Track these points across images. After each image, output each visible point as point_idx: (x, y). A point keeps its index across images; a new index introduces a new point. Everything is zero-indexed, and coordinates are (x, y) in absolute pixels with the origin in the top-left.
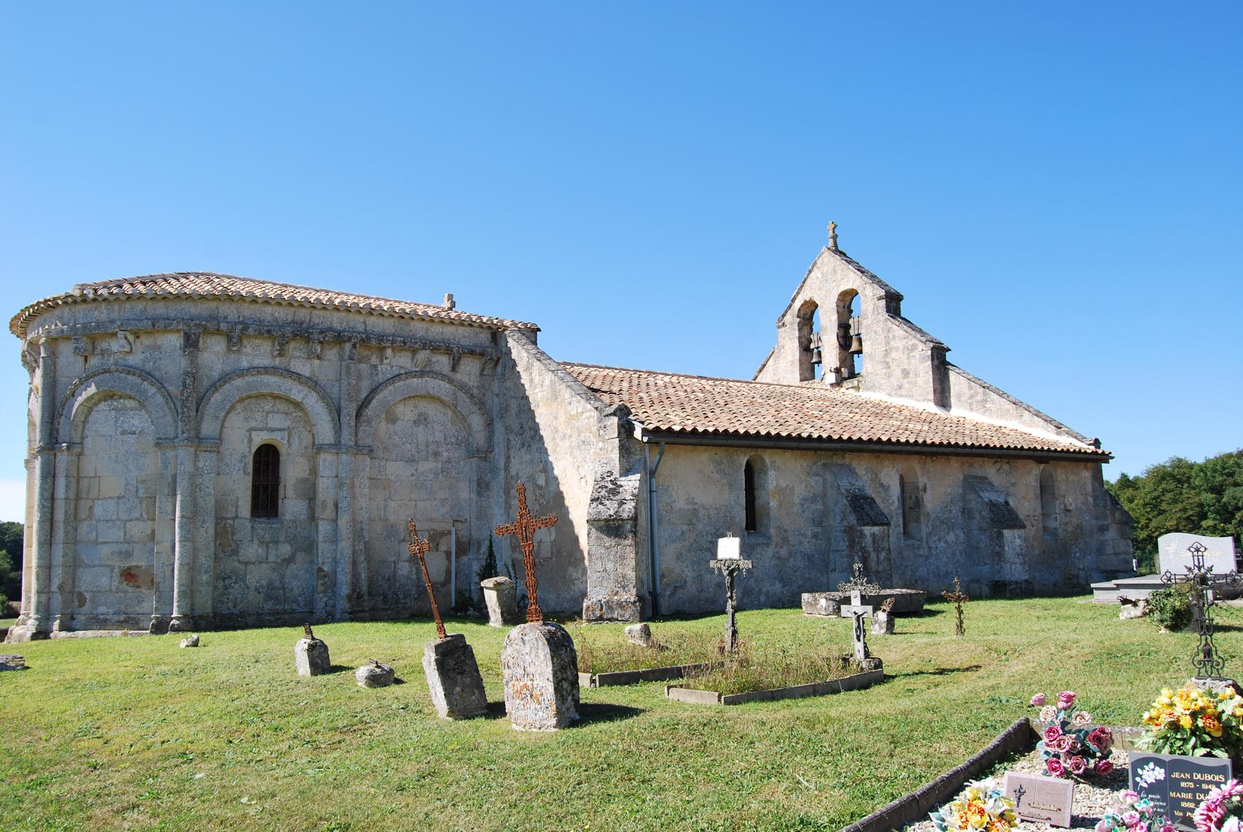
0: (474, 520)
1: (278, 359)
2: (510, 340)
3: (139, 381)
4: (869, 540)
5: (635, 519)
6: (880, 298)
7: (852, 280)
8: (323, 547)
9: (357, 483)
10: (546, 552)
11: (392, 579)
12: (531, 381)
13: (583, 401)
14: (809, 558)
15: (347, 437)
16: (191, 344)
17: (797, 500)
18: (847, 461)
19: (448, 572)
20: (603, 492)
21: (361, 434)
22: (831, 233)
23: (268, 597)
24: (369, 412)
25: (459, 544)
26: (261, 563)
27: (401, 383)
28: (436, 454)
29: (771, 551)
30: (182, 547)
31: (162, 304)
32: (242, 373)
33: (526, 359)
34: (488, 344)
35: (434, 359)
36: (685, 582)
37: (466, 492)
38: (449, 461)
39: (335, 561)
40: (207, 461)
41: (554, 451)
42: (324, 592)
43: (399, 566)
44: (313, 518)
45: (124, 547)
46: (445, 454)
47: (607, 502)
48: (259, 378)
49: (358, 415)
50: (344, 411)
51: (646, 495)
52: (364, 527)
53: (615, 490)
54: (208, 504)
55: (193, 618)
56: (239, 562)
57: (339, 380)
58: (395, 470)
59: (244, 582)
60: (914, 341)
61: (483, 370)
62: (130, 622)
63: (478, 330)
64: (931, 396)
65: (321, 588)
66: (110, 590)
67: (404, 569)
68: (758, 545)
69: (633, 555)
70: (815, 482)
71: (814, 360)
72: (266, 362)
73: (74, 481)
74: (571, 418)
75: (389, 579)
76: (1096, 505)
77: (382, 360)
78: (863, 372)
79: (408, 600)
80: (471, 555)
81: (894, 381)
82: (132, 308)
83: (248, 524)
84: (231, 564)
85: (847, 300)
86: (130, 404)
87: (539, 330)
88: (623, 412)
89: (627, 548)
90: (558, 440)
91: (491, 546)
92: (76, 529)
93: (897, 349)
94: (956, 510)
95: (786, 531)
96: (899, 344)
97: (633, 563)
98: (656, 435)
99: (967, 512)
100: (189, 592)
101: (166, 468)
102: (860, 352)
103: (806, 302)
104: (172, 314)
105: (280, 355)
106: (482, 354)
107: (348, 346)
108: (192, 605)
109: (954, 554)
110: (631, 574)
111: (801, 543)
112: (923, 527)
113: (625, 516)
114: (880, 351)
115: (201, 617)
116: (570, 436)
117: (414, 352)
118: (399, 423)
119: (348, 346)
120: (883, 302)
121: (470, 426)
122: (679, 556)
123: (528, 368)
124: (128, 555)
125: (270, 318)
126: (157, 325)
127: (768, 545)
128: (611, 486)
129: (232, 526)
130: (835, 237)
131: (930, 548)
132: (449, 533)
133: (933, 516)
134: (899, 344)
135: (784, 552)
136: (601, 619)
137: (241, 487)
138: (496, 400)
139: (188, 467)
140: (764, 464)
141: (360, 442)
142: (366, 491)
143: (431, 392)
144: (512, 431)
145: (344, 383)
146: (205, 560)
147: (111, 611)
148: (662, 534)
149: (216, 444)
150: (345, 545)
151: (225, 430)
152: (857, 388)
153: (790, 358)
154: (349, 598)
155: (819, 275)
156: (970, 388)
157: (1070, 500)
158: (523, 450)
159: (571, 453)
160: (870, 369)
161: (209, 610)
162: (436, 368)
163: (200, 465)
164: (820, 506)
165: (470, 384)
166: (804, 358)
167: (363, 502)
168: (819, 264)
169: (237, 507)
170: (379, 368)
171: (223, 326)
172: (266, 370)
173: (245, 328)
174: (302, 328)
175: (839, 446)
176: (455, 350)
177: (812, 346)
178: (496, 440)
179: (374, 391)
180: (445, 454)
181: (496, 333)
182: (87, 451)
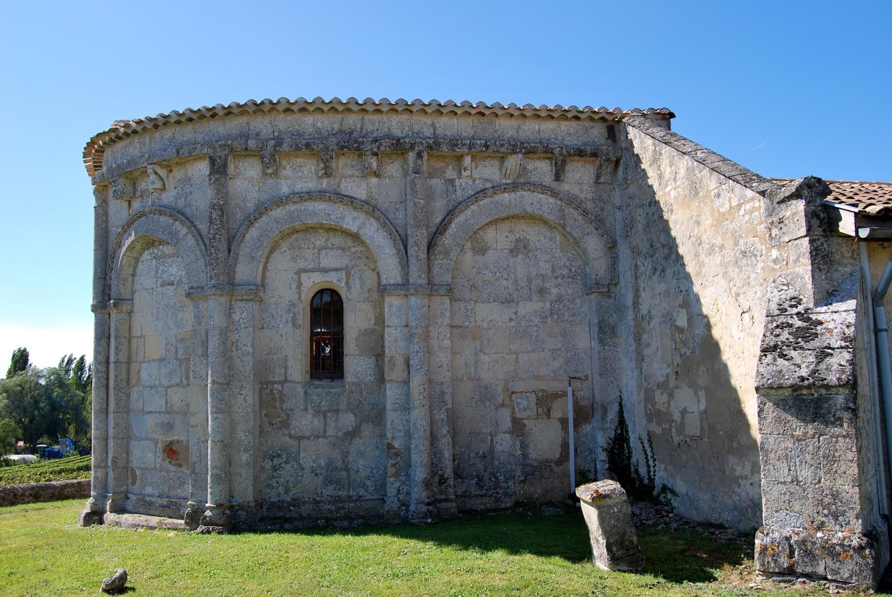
0: (596, 376)
1: (325, 181)
2: (630, 129)
3: (171, 221)
5: (852, 384)
8: (391, 417)
9: (434, 332)
10: (693, 428)
11: (487, 456)
12: (660, 176)
15: (417, 275)
16: (219, 169)
19: (565, 446)
21: (436, 270)
23: (328, 481)
24: (446, 240)
26: (317, 437)
27: (487, 201)
28: (542, 291)
30: (214, 420)
31: (189, 127)
32: (281, 201)
33: (651, 148)
34: (603, 141)
35: (530, 166)
37: (584, 340)
38: (560, 299)
39: (408, 435)
40: (242, 313)
41: (698, 274)
42: (396, 475)
43: (498, 438)
44: (381, 379)
45: (166, 418)
46: (554, 291)
47: (793, 353)
48: (302, 206)
49: (431, 246)
50: (411, 241)
52: (446, 390)
53: (808, 330)
54: (246, 365)
55: (231, 507)
56: (290, 436)
57: (404, 202)
58: (487, 314)
59: (297, 461)
61: (598, 176)
62: (170, 509)
63: (587, 124)
65: (391, 471)
66: (155, 469)
67: (504, 443)
72: (311, 185)
73: (125, 342)
75: (484, 457)
77: (460, 173)
79: (511, 483)
80: (595, 423)
82: (162, 137)
83: (301, 390)
84: (281, 440)
86: (168, 249)
87: (672, 115)
90: (702, 257)
92: (128, 396)
97: (854, 470)
100: (225, 475)
101: (200, 323)
104: (200, 138)
105: (328, 175)
106: (594, 155)
107: (411, 156)
108: (231, 491)
110: (851, 492)
113: (832, 378)
115: (241, 507)
116: (722, 247)
117: (502, 159)
118: (490, 254)
119: (411, 156)
121: (585, 251)
123: (655, 160)
124: (169, 427)
125: (311, 130)
126: (182, 155)
128: (798, 323)
129: (281, 392)
136: (789, 573)
137: (293, 346)
138: (618, 214)
139: (218, 320)
141: (436, 280)
142: (447, 343)
143: (529, 210)
144: (639, 253)
145: (410, 204)
146: (244, 436)
147: (156, 492)
149: (257, 291)
150: (419, 415)
151: (268, 274)
154: (427, 484)
158: (655, 278)
159: (725, 274)
161: (251, 498)
162: (534, 178)
163: (236, 317)
165: (582, 196)
167: (443, 358)
169: (286, 368)
170: (457, 183)
171: (252, 144)
172: (310, 196)
173: (279, 143)
174: (349, 136)
176: (557, 151)
178: (621, 268)
179: (451, 214)
180: (554, 291)
181: (613, 125)
182: (136, 308)
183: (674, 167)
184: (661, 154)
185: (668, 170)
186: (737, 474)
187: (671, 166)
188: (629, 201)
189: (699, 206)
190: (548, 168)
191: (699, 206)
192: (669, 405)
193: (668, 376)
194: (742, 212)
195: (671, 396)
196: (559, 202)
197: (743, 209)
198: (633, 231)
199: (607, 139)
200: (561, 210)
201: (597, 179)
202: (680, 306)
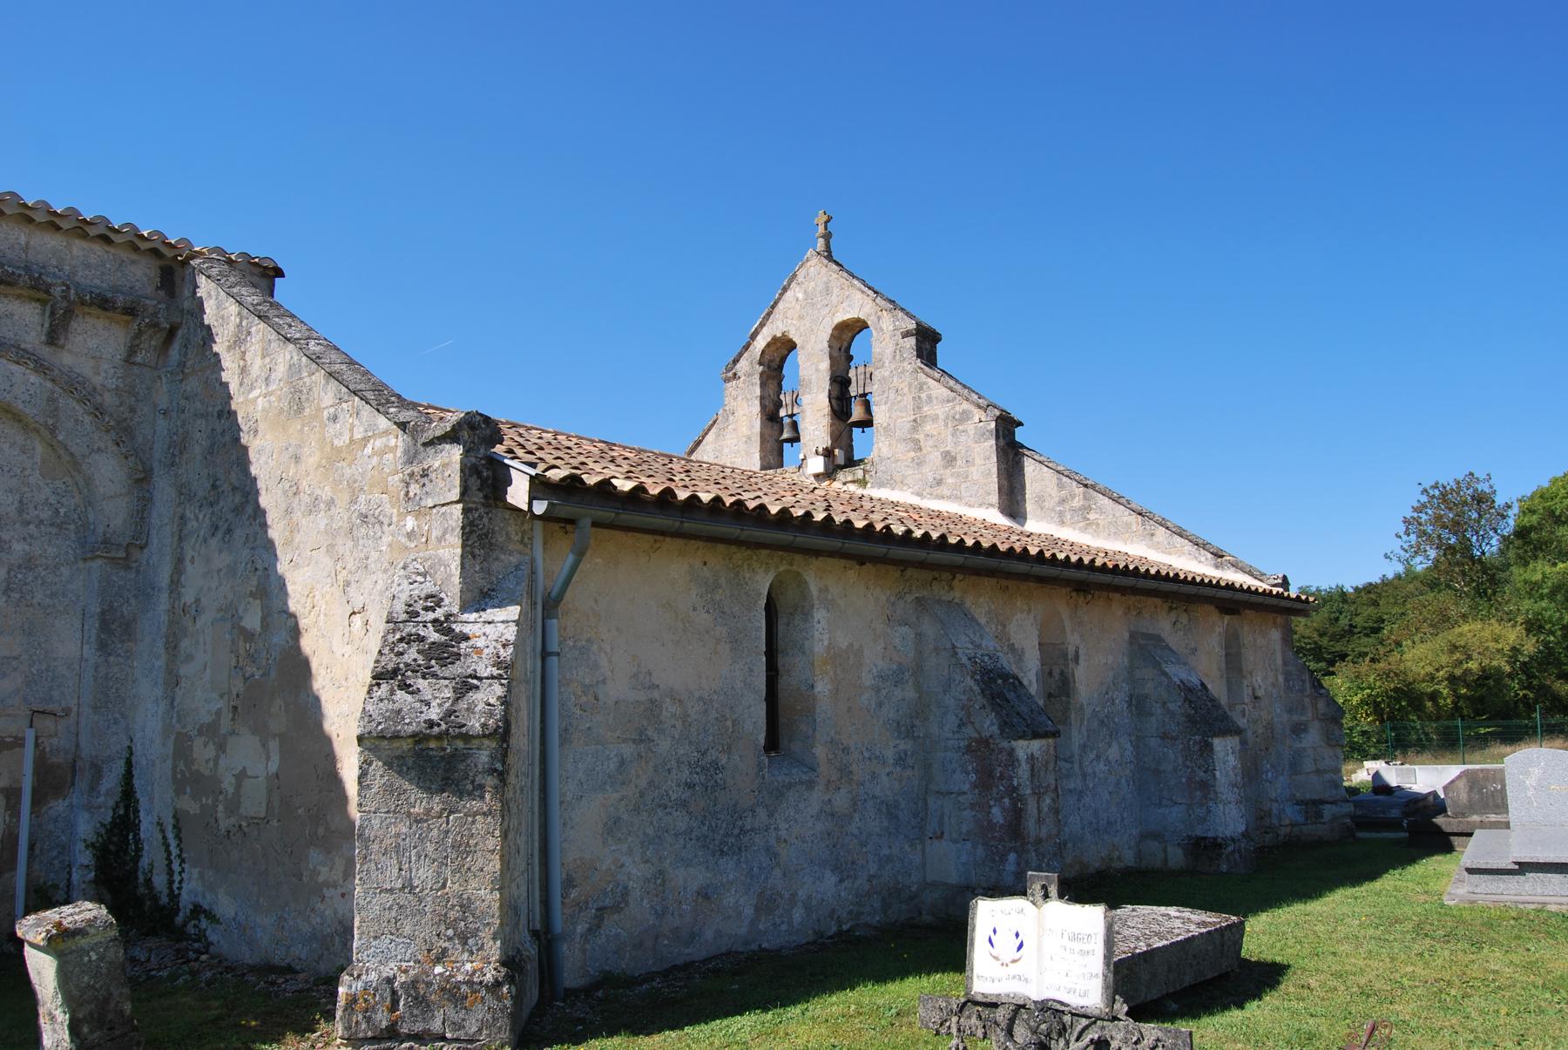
2: (202, 280)
4: (1023, 771)
5: (502, 734)
6: (906, 335)
7: (856, 304)
10: (254, 803)
12: (244, 370)
13: (367, 410)
14: (890, 810)
17: (868, 680)
18: (956, 595)
20: (412, 654)
22: (821, 229)
25: (43, 768)
29: (817, 796)
33: (234, 320)
34: (150, 290)
36: (626, 892)
37: (69, 643)
38: (28, 563)
41: (288, 543)
46: (18, 547)
47: (421, 684)
51: (532, 664)
53: (446, 649)
60: (966, 406)
61: (132, 350)
63: (125, 255)
64: (995, 498)
68: (790, 786)
69: (493, 843)
70: (902, 636)
71: (785, 435)
74: (335, 457)
76: (1289, 689)
78: (873, 455)
81: (928, 473)
85: (847, 335)
87: (279, 273)
88: (478, 434)
89: (482, 830)
90: (297, 516)
91: (129, 775)
93: (935, 418)
94: (1120, 698)
95: (846, 750)
96: (941, 410)
97: (495, 865)
98: (577, 503)
99: (1138, 704)
102: (867, 423)
103: (775, 339)
106: (131, 311)
109: (1118, 784)
110: (487, 898)
111: (874, 776)
112: (1075, 733)
113: (475, 724)
114: (905, 421)
116: (330, 504)
120: (912, 341)
121: (89, 481)
122: (612, 827)
123: (238, 342)
127: (810, 785)
128: (434, 636)
130: (827, 237)
131: (1084, 775)
132: (19, 742)
133: (1088, 711)
134: (941, 410)
135: (841, 801)
138: (162, 423)
140: (805, 595)
148: (568, 769)
152: (862, 483)
153: (744, 430)
155: (800, 296)
156: (1061, 486)
157: (1258, 679)
158: (213, 542)
160: (885, 451)
164: (910, 694)
165: (97, 380)
166: (768, 432)
168: (800, 278)
175: (958, 559)
176: (57, 291)
177: (782, 413)
180: (18, 547)
181: (172, 268)
183: (267, 360)
184: (249, 333)
185: (258, 361)
186: (321, 879)
187: (263, 357)
188: (183, 402)
189: (302, 430)
190: (37, 319)
191: (302, 430)
192: (216, 764)
193: (218, 713)
194: (368, 450)
195: (221, 748)
196: (49, 385)
197: (370, 446)
198: (185, 456)
199: (158, 288)
200: (52, 400)
201: (130, 356)
202: (252, 594)
